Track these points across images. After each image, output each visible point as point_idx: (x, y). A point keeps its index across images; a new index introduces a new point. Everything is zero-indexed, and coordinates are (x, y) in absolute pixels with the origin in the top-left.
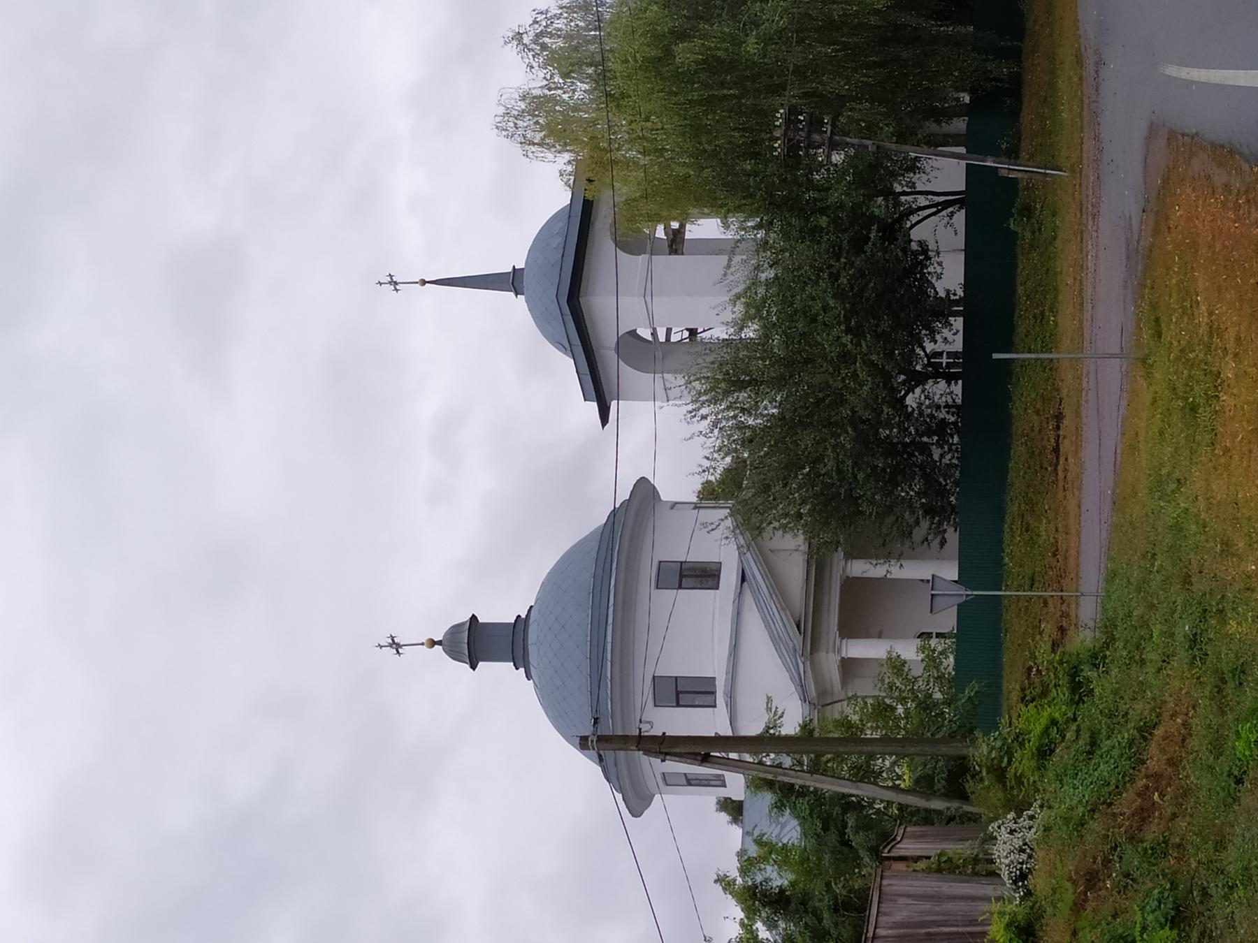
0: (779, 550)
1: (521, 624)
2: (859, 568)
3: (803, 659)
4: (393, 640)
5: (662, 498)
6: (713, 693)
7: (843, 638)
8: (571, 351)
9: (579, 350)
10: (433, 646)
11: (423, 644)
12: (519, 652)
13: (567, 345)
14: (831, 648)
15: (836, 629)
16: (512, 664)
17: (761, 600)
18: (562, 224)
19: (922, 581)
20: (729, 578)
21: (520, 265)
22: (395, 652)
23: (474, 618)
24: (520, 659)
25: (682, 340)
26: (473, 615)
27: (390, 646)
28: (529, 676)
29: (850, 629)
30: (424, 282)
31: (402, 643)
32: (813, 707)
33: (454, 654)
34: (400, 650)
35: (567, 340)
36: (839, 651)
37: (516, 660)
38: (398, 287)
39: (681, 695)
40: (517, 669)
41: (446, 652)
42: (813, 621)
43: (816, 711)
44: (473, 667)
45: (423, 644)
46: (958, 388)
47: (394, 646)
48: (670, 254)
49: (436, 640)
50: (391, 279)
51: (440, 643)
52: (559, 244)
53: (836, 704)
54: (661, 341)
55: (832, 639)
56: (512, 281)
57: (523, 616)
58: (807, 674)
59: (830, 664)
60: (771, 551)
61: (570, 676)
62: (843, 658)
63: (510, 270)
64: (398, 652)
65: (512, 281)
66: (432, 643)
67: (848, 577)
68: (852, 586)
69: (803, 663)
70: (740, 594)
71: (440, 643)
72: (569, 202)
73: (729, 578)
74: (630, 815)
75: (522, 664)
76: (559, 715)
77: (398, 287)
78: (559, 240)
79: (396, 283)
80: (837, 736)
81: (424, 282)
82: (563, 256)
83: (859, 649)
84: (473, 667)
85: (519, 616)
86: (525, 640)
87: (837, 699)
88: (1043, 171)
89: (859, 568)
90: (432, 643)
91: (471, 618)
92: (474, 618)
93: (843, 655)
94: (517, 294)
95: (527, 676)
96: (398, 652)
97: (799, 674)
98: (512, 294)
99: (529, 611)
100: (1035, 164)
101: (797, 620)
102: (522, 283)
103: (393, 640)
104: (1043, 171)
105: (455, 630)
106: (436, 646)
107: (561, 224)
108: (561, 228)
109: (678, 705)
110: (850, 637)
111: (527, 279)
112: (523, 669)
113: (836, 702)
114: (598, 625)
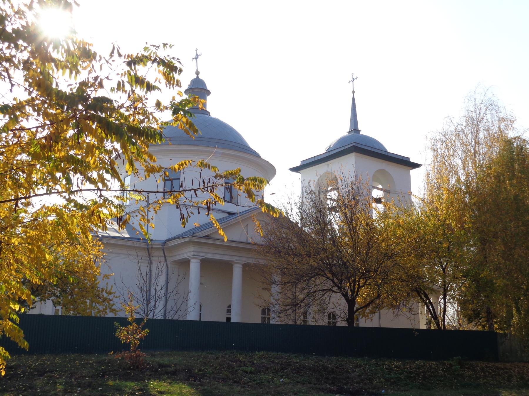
2: (237, 272)
9: (327, 155)
14: (196, 254)
19: (230, 306)
21: (361, 133)
29: (205, 263)
30: (353, 92)
34: (195, 59)
36: (194, 258)
39: (170, 182)
46: (344, 324)
51: (198, 77)
55: (201, 254)
59: (187, 253)
66: (197, 73)
67: (232, 265)
68: (227, 267)
70: (223, 211)
71: (198, 77)
80: (128, 383)
81: (353, 92)
83: (194, 267)
89: (237, 272)
90: (197, 73)
93: (192, 260)
96: (193, 59)
110: (201, 264)
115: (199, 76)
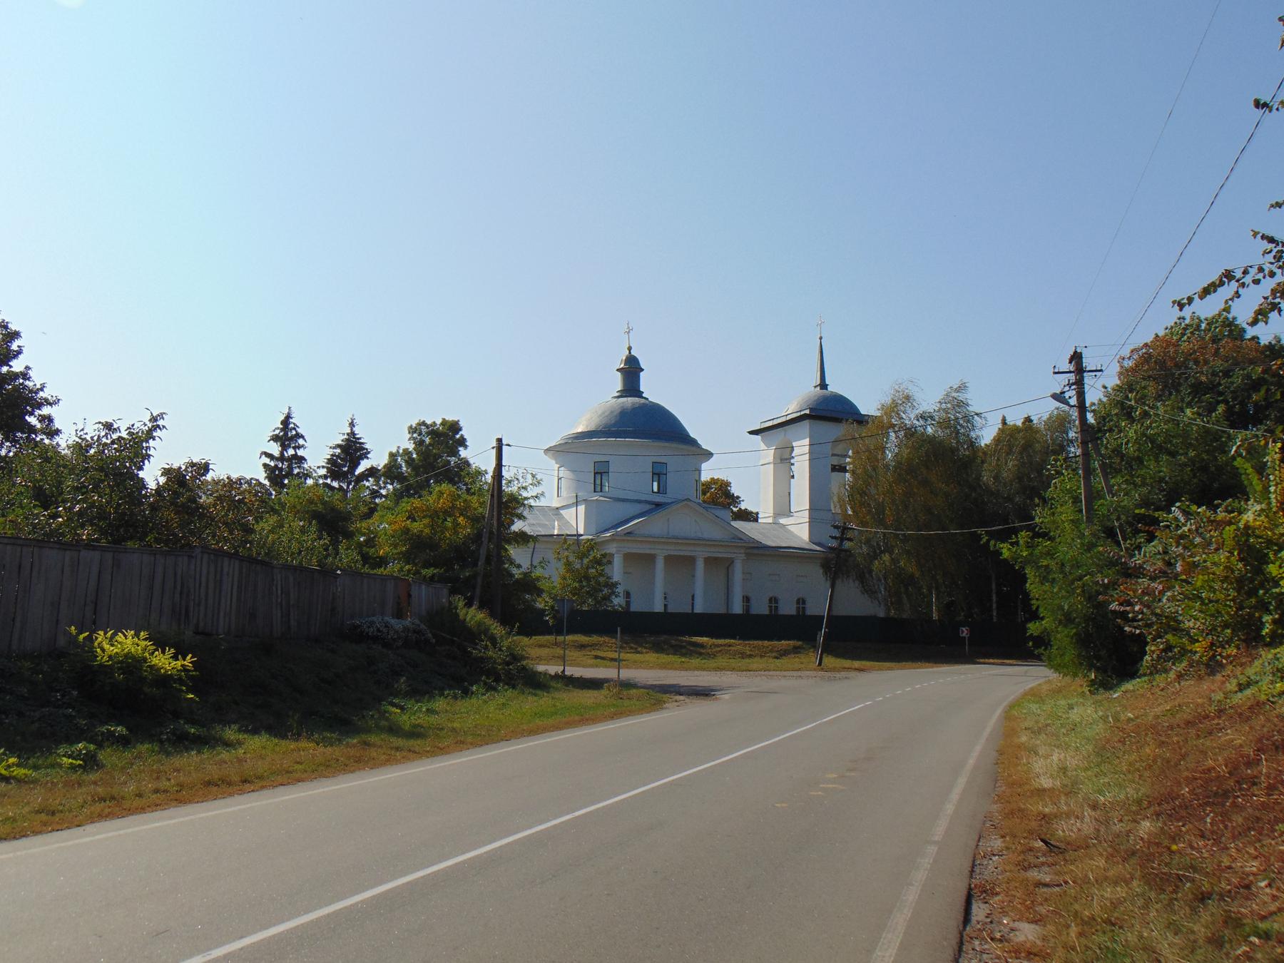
6: (601, 491)
30: (821, 338)
51: (630, 353)
57: (644, 395)
62: (613, 555)
66: (630, 349)
68: (650, 559)
71: (630, 353)
81: (821, 338)
90: (630, 349)
99: (645, 398)
109: (595, 474)
115: (632, 351)
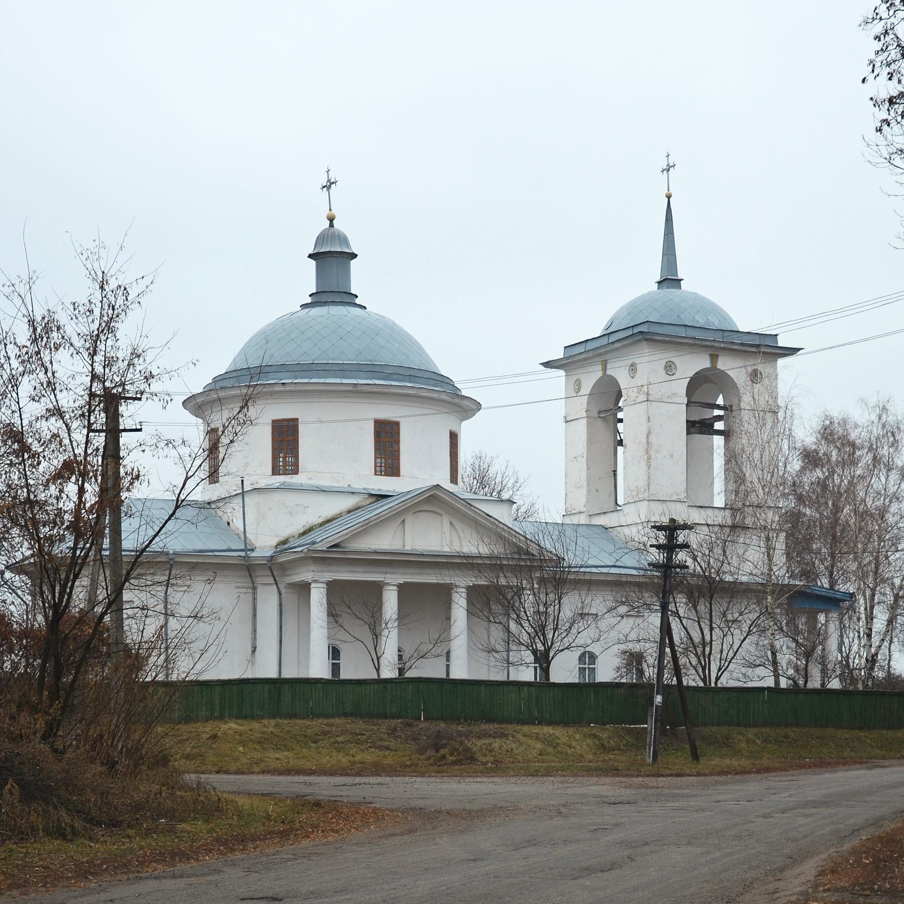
0: (404, 529)
1: (348, 298)
3: (305, 551)
4: (333, 183)
5: (463, 422)
7: (467, 589)
8: (604, 335)
10: (328, 219)
11: (330, 210)
12: (323, 298)
13: (609, 331)
15: (333, 578)
16: (315, 292)
17: (364, 512)
18: (716, 323)
20: (385, 484)
22: (324, 185)
23: (354, 256)
24: (320, 298)
25: (619, 433)
26: (357, 255)
27: (329, 181)
28: (304, 306)
31: (330, 190)
32: (269, 559)
33: (322, 239)
35: (612, 331)
37: (317, 294)
38: (665, 172)
40: (310, 296)
41: (324, 231)
42: (415, 561)
43: (265, 562)
44: (310, 256)
45: (330, 210)
47: (328, 184)
48: (687, 421)
49: (334, 222)
50: (672, 166)
51: (331, 225)
52: (698, 321)
53: (273, 579)
54: (618, 414)
56: (670, 281)
57: (357, 301)
58: (294, 554)
60: (404, 520)
61: (316, 345)
62: (310, 584)
63: (680, 276)
64: (324, 187)
65: (670, 281)
66: (331, 220)
67: (382, 587)
68: (444, 593)
69: (302, 551)
71: (331, 225)
72: (740, 330)
73: (385, 484)
74: (183, 401)
75: (314, 301)
76: (265, 338)
77: (665, 172)
78: (701, 321)
79: (668, 170)
82: (686, 326)
84: (310, 256)
85: (356, 297)
86: (334, 303)
87: (277, 580)
88: (652, 744)
90: (331, 220)
91: (353, 253)
92: (354, 256)
93: (313, 585)
94: (659, 283)
95: (302, 305)
96: (324, 187)
97: (295, 547)
98: (658, 279)
100: (657, 737)
101: (342, 545)
102: (667, 288)
103: (333, 183)
104: (652, 744)
105: (343, 240)
106: (329, 222)
107: (716, 323)
108: (713, 323)
110: (399, 592)
111: (670, 293)
112: (310, 301)
113: (275, 580)
114: (342, 370)
